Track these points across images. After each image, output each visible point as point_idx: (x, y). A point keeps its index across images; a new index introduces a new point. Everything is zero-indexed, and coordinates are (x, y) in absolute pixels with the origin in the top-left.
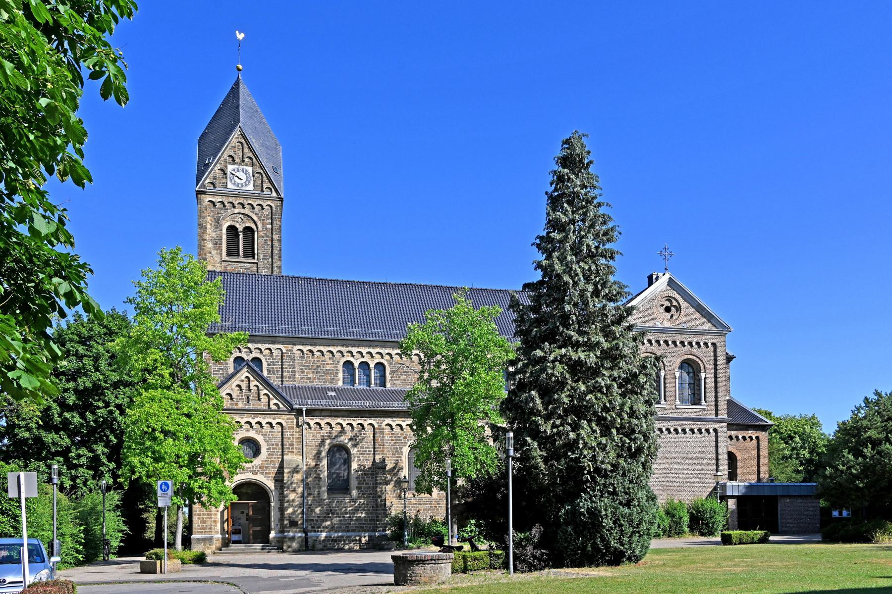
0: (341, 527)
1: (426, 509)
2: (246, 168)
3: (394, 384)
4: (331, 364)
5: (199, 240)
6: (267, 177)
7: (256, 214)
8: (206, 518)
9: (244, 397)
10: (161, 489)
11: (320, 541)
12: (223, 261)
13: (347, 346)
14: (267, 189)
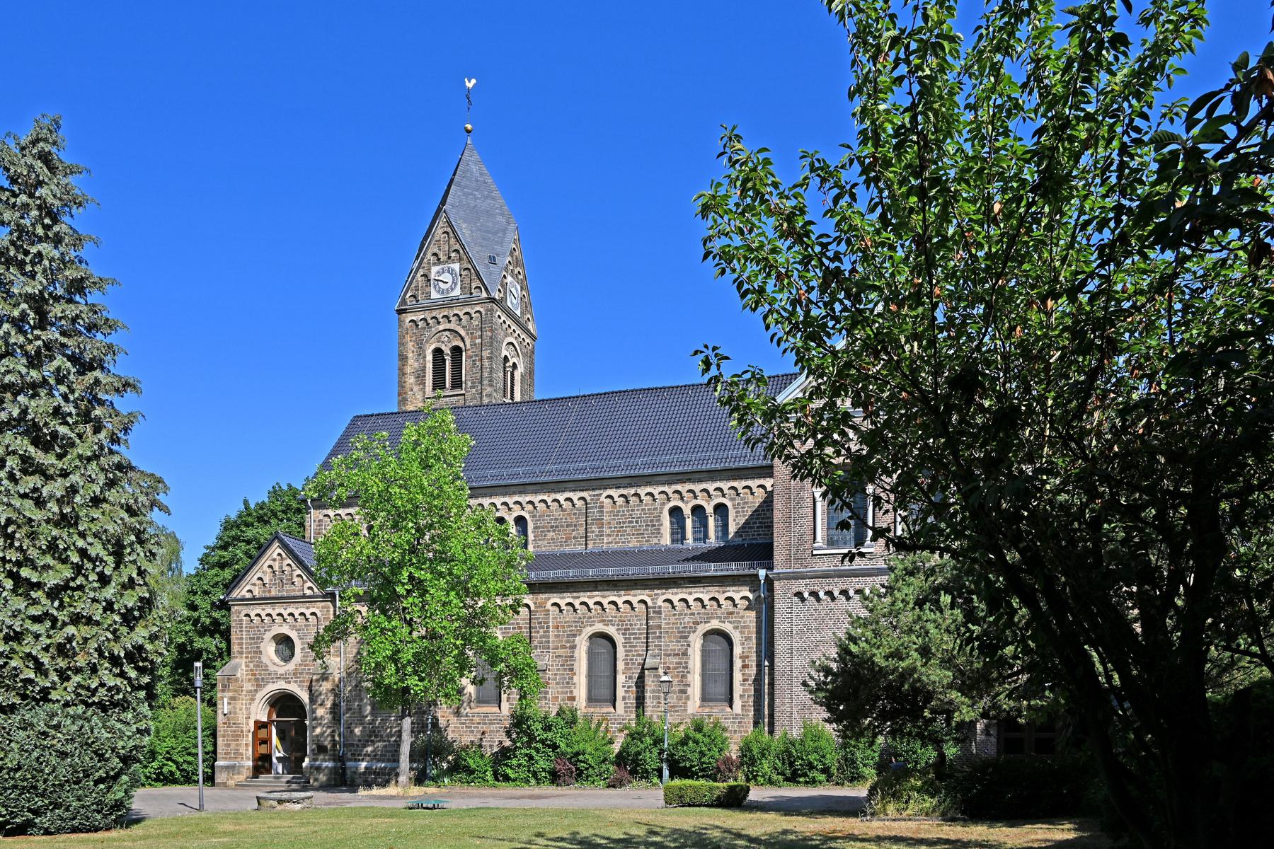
2: (452, 266)
11: (360, 774)
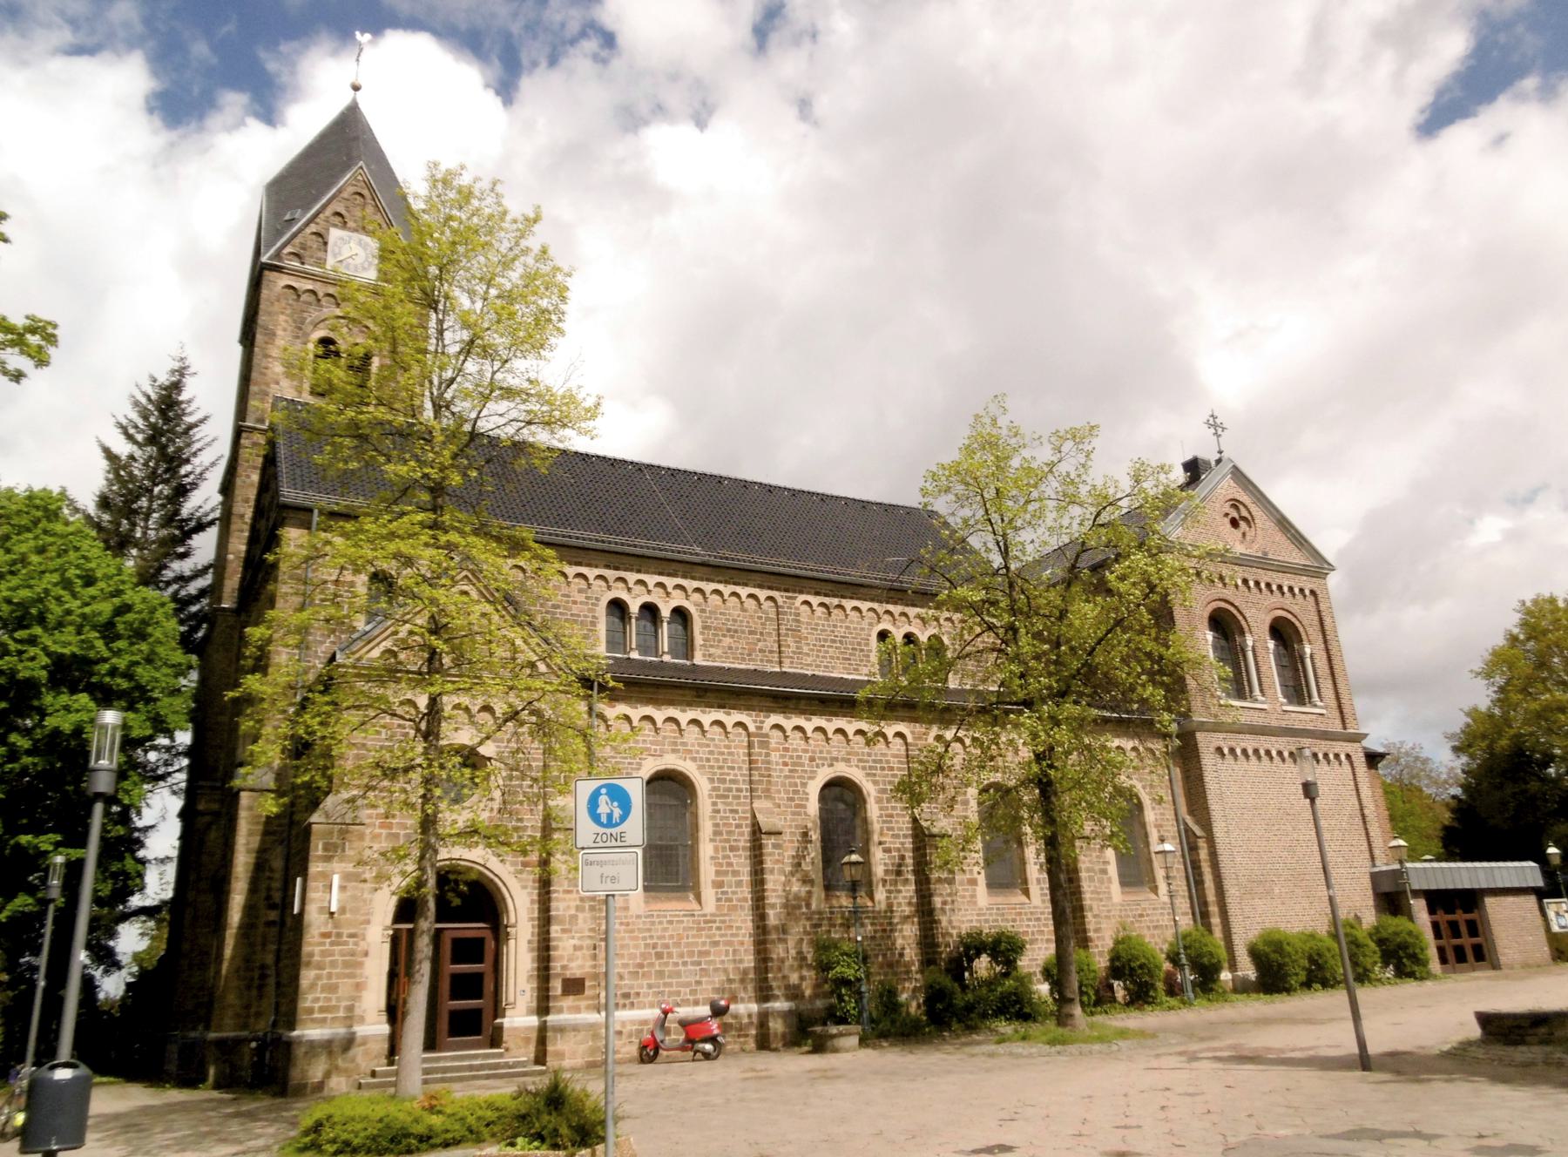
3: (710, 655)
4: (581, 603)
8: (339, 976)
10: (596, 818)
13: (617, 568)
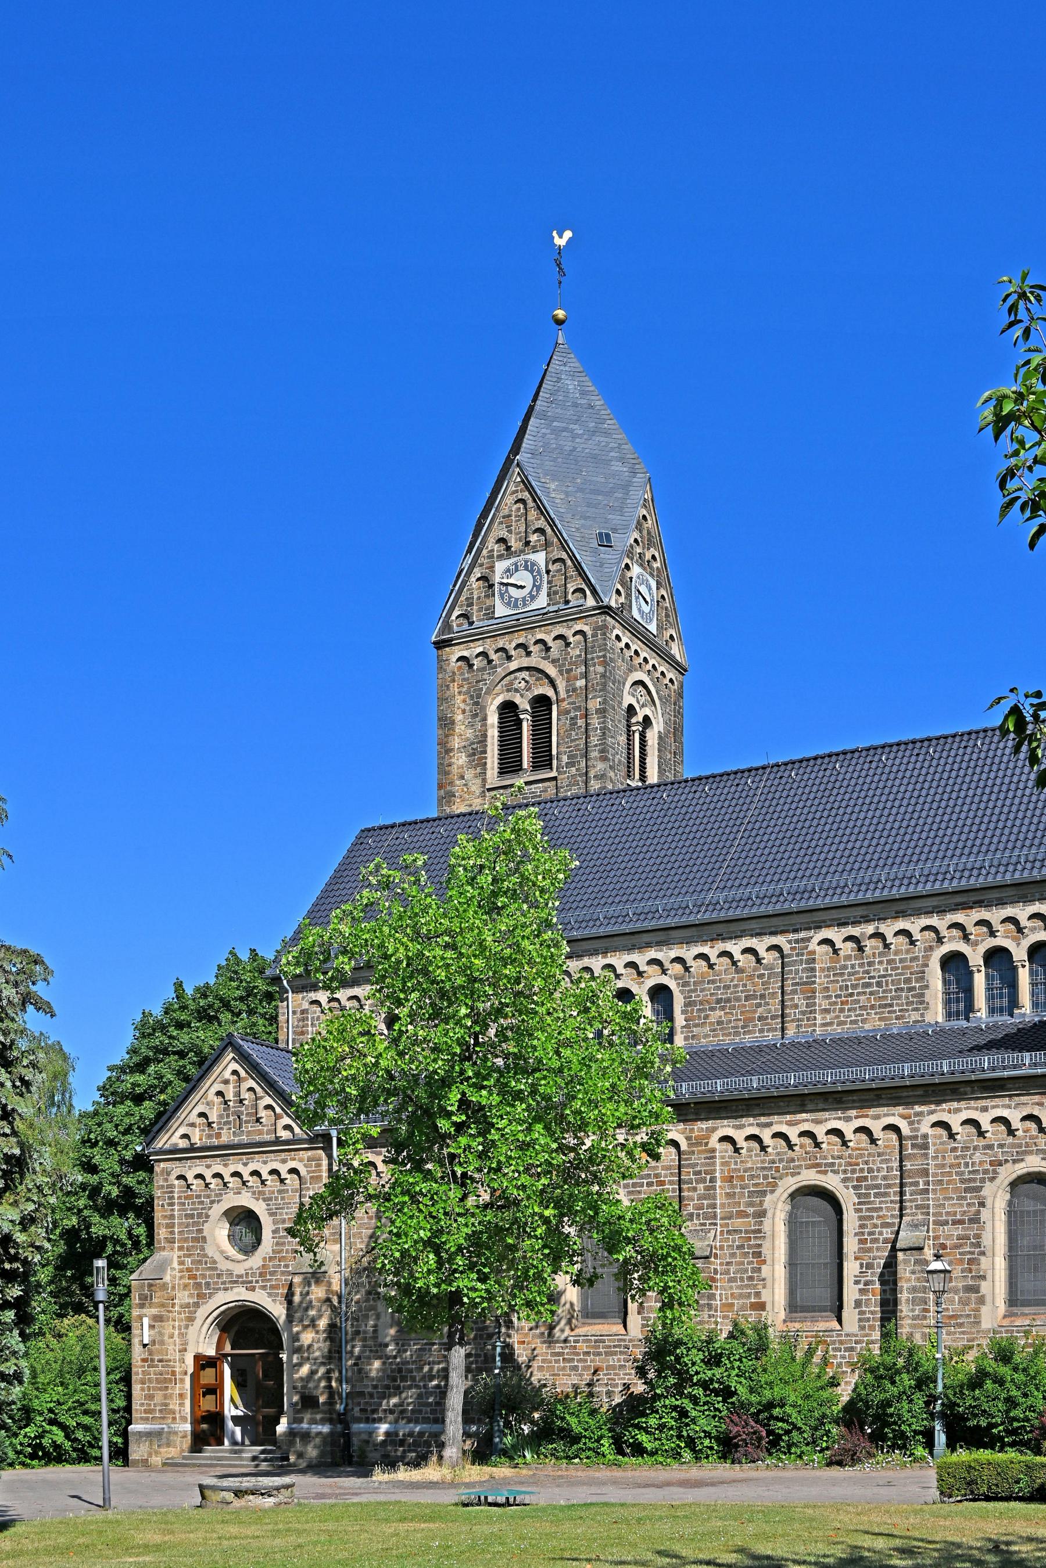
0: (420, 1412)
1: (613, 1367)
5: (439, 753)
6: (575, 566)
7: (554, 661)
8: (154, 1389)
9: (231, 1118)
11: (375, 1445)
12: (489, 790)
14: (577, 594)
